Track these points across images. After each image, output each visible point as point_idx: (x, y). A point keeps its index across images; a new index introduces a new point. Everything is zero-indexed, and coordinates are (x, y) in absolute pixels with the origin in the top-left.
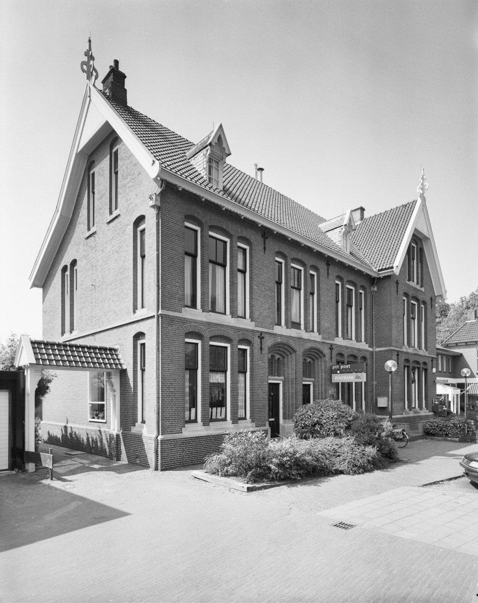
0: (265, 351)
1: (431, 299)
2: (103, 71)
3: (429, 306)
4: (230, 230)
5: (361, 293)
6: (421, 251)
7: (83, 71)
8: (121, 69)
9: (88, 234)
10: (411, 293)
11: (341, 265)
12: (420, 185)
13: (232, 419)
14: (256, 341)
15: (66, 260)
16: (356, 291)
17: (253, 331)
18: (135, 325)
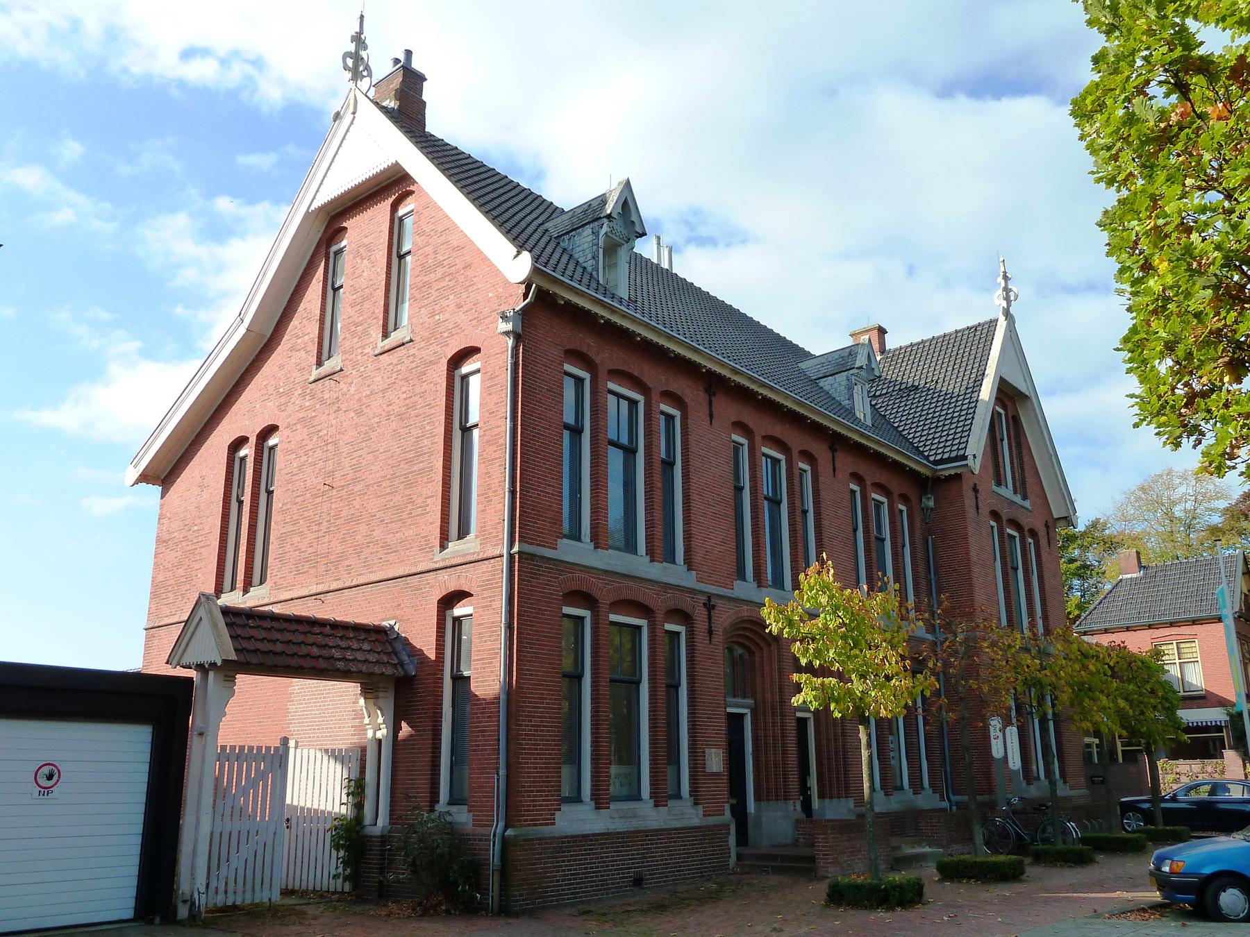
0: (719, 637)
1: (1047, 526)
2: (381, 65)
3: (1043, 542)
4: (592, 354)
5: (901, 511)
6: (1015, 421)
7: (346, 68)
8: (416, 65)
9: (315, 373)
10: (1005, 513)
11: (859, 450)
12: (1000, 292)
13: (654, 795)
14: (700, 614)
15: (242, 420)
16: (752, 449)
17: (693, 591)
18: (443, 576)
